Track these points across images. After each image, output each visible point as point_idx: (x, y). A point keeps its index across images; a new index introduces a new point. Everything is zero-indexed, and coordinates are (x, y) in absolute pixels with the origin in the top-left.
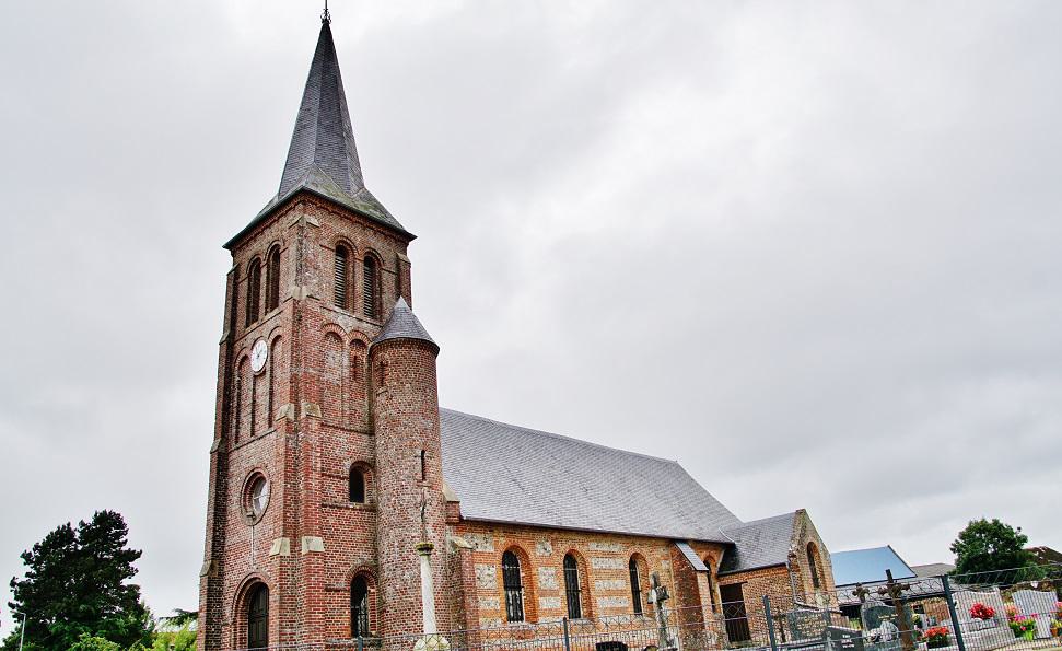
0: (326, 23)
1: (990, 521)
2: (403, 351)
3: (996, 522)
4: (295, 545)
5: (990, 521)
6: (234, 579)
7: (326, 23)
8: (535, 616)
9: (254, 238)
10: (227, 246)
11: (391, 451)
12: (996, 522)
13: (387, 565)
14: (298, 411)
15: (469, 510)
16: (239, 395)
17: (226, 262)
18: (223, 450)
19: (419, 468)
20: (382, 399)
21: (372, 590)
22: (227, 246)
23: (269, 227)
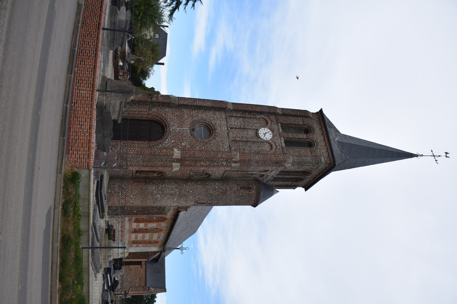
0: (417, 156)
1: (155, 299)
2: (254, 198)
3: (155, 301)
4: (177, 160)
5: (155, 299)
6: (169, 115)
7: (417, 156)
8: (137, 222)
9: (321, 129)
10: (321, 111)
11: (211, 192)
12: (155, 301)
13: (164, 186)
14: (235, 162)
15: (182, 214)
16: (251, 118)
17: (314, 109)
18: (227, 109)
19: (203, 202)
20: (235, 187)
21: (155, 175)
22: (321, 111)
23: (327, 151)
